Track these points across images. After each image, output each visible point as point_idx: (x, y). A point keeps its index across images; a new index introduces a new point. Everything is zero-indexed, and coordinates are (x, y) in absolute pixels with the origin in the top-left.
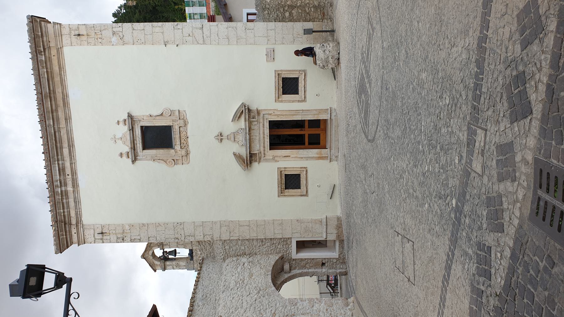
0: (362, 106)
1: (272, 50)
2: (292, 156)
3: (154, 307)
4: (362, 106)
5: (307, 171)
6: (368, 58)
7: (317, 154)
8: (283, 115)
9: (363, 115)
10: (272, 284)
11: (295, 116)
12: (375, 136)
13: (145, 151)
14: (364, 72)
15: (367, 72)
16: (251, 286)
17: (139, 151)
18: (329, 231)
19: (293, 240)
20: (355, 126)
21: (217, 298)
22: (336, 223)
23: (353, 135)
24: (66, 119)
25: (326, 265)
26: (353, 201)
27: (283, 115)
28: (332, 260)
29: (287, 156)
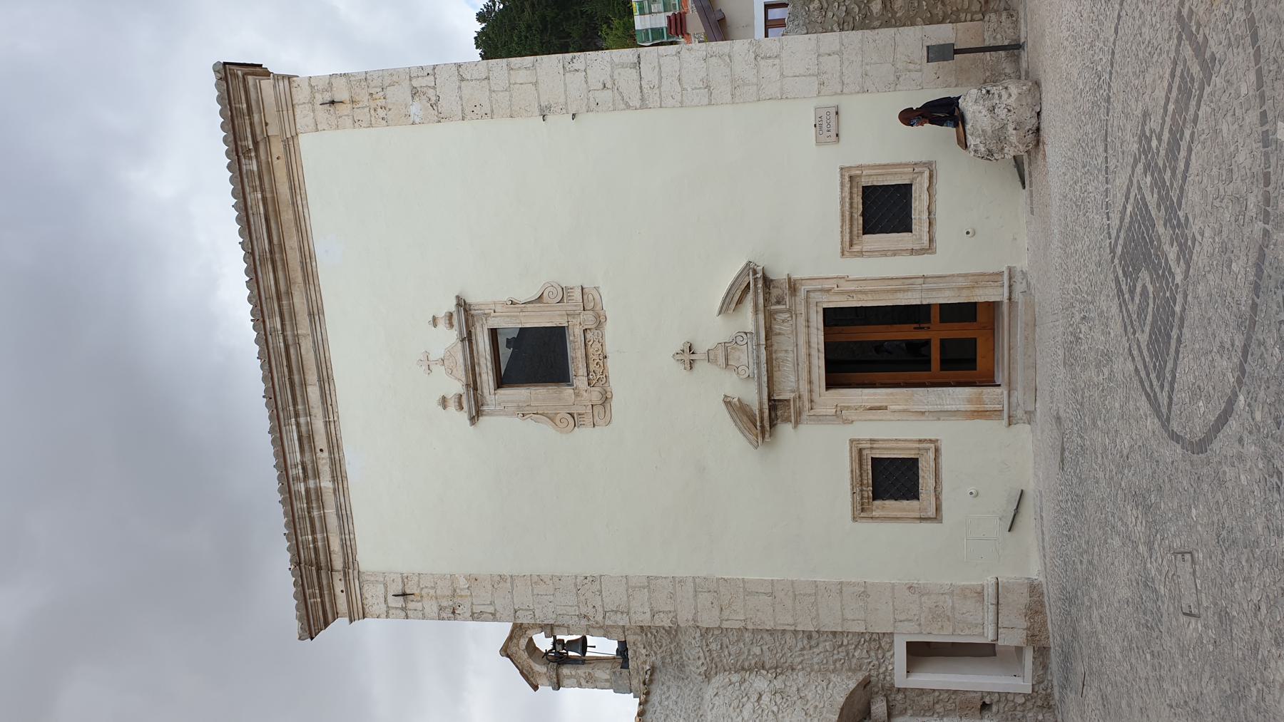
1: (833, 111)
5: (937, 450)
7: (970, 401)
11: (900, 295)
17: (486, 392)
28: (1010, 697)
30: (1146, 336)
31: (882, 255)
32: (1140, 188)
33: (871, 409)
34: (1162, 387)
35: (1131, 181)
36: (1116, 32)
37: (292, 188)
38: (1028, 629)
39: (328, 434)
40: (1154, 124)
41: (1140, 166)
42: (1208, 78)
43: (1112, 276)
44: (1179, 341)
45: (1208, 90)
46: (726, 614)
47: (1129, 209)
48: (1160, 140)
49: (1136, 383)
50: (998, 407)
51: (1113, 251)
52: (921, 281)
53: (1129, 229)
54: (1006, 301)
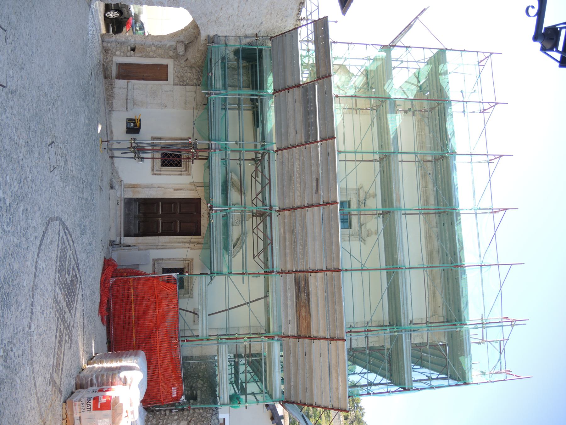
0: (69, 265)
1: (196, 322)
2: (172, 190)
3: (344, 13)
4: (69, 265)
5: (153, 170)
6: (61, 337)
7: (138, 192)
8: (183, 242)
9: (69, 253)
10: (200, 28)
11: (168, 241)
12: (46, 228)
13: (166, 64)
14: (68, 314)
15: (62, 316)
16: (227, 27)
17: (355, 200)
18: (125, 91)
19: (172, 83)
20: (82, 234)
21: (268, 16)
22: (115, 101)
23: (87, 222)
24: (430, 237)
25: (129, 48)
26: (88, 130)
27: (183, 242)
28: (122, 54)
29: (178, 189)
30: (68, 254)
31: (175, 259)
32: (71, 316)
33: (181, 189)
34: (73, 269)
35: (75, 317)
36: (38, 255)
37: (434, 293)
38: (114, 88)
39: (426, 182)
40: (68, 345)
41: (71, 325)
42: (51, 377)
43: (81, 270)
44: (56, 262)
45: (51, 371)
46: (250, 398)
47: (75, 305)
48: (65, 340)
49: (71, 231)
50: (125, 189)
51: (81, 282)
52: (159, 247)
53: (75, 296)
54: (122, 237)
